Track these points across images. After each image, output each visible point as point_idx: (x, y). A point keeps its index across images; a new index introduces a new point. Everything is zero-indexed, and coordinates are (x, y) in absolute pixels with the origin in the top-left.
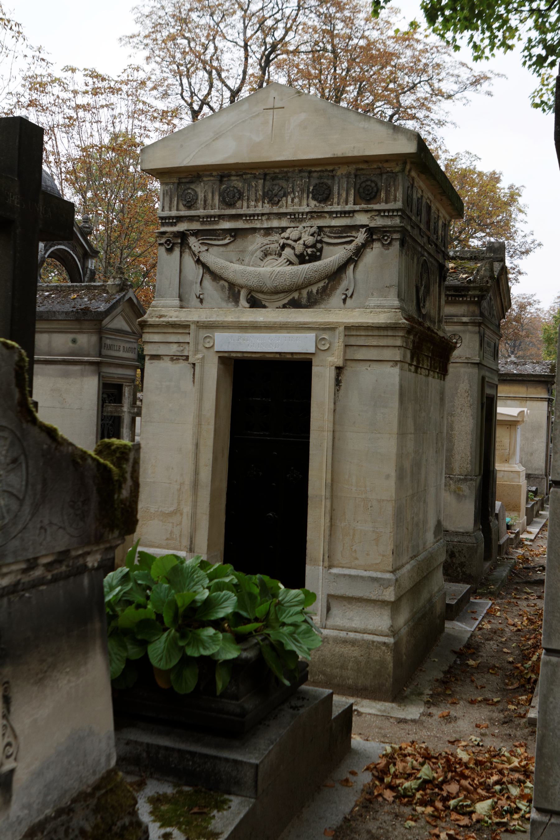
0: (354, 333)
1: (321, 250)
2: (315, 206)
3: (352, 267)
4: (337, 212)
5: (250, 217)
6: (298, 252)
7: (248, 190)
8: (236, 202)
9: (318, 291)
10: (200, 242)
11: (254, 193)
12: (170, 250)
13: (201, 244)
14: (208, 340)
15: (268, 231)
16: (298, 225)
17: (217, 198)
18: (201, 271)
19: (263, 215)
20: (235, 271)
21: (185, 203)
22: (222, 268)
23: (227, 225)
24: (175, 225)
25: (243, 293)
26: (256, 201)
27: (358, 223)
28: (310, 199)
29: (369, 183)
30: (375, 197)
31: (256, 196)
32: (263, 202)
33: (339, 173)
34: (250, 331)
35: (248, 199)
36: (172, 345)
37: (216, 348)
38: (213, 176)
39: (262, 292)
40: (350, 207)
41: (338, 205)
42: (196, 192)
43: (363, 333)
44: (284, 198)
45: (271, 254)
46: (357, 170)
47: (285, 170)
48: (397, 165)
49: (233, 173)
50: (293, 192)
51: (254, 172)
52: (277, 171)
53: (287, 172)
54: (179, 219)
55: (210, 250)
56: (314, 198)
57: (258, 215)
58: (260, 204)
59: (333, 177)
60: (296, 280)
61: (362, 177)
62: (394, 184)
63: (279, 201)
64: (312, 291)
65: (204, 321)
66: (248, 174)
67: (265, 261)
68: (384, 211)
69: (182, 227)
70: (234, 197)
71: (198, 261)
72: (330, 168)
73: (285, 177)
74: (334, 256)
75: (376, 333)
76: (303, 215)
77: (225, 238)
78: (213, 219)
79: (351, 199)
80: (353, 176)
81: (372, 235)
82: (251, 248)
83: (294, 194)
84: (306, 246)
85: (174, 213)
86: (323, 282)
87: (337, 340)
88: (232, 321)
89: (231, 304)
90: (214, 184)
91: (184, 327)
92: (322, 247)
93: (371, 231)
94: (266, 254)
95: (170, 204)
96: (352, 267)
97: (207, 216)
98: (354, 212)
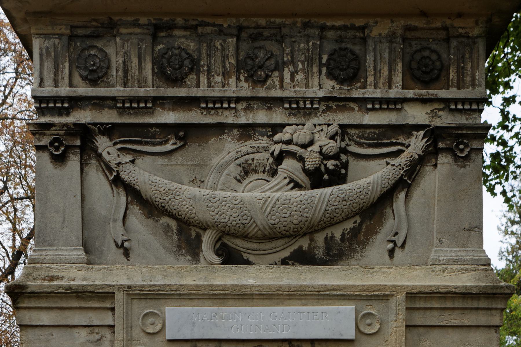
0: (421, 305)
1: (345, 166)
2: (333, 88)
3: (402, 195)
4: (373, 100)
5: (214, 103)
6: (309, 165)
7: (209, 56)
8: (186, 75)
9: (343, 235)
10: (119, 146)
11: (219, 61)
12: (60, 160)
13: (119, 150)
14: (151, 320)
15: (247, 131)
16: (303, 120)
17: (148, 67)
18: (123, 199)
19: (238, 100)
20: (193, 198)
21: (85, 73)
22: (168, 192)
23: (169, 117)
24: (68, 115)
25: (207, 239)
26: (223, 75)
27: (411, 121)
28: (323, 77)
29: (427, 53)
30: (437, 79)
31: (224, 67)
32: (238, 79)
33: (375, 32)
34: (231, 302)
35: (209, 72)
36: (76, 330)
37: (169, 335)
38: (139, 26)
39: (245, 237)
40: (395, 92)
41: (375, 88)
42: (106, 57)
43: (436, 305)
44: (276, 74)
45: (256, 171)
46: (408, 28)
47: (278, 20)
48: (477, 23)
49: (180, 21)
50: (293, 62)
51: (219, 21)
52: (262, 22)
53: (279, 27)
54: (76, 102)
55: (138, 161)
56: (331, 75)
57: (229, 100)
58: (232, 81)
59: (364, 40)
60: (310, 215)
61: (413, 43)
62: (471, 57)
63: (267, 77)
64: (332, 237)
65: (143, 286)
66: (208, 24)
67: (245, 182)
68: (456, 101)
69: (83, 116)
70: (181, 67)
71: (118, 182)
72: (359, 22)
73: (275, 35)
74: (370, 176)
75: (458, 304)
76: (312, 103)
77: (166, 142)
78: (142, 105)
79: (398, 78)
80: (399, 40)
81: (435, 143)
82: (216, 161)
83: (295, 66)
84: (325, 156)
85: (64, 90)
86: (353, 220)
87: (392, 317)
88: (197, 286)
89: (184, 261)
90: (142, 40)
91: (103, 296)
92: (347, 162)
93: (434, 134)
94: (247, 171)
95: (56, 74)
96: (402, 195)
97: (132, 99)
98: (405, 100)
